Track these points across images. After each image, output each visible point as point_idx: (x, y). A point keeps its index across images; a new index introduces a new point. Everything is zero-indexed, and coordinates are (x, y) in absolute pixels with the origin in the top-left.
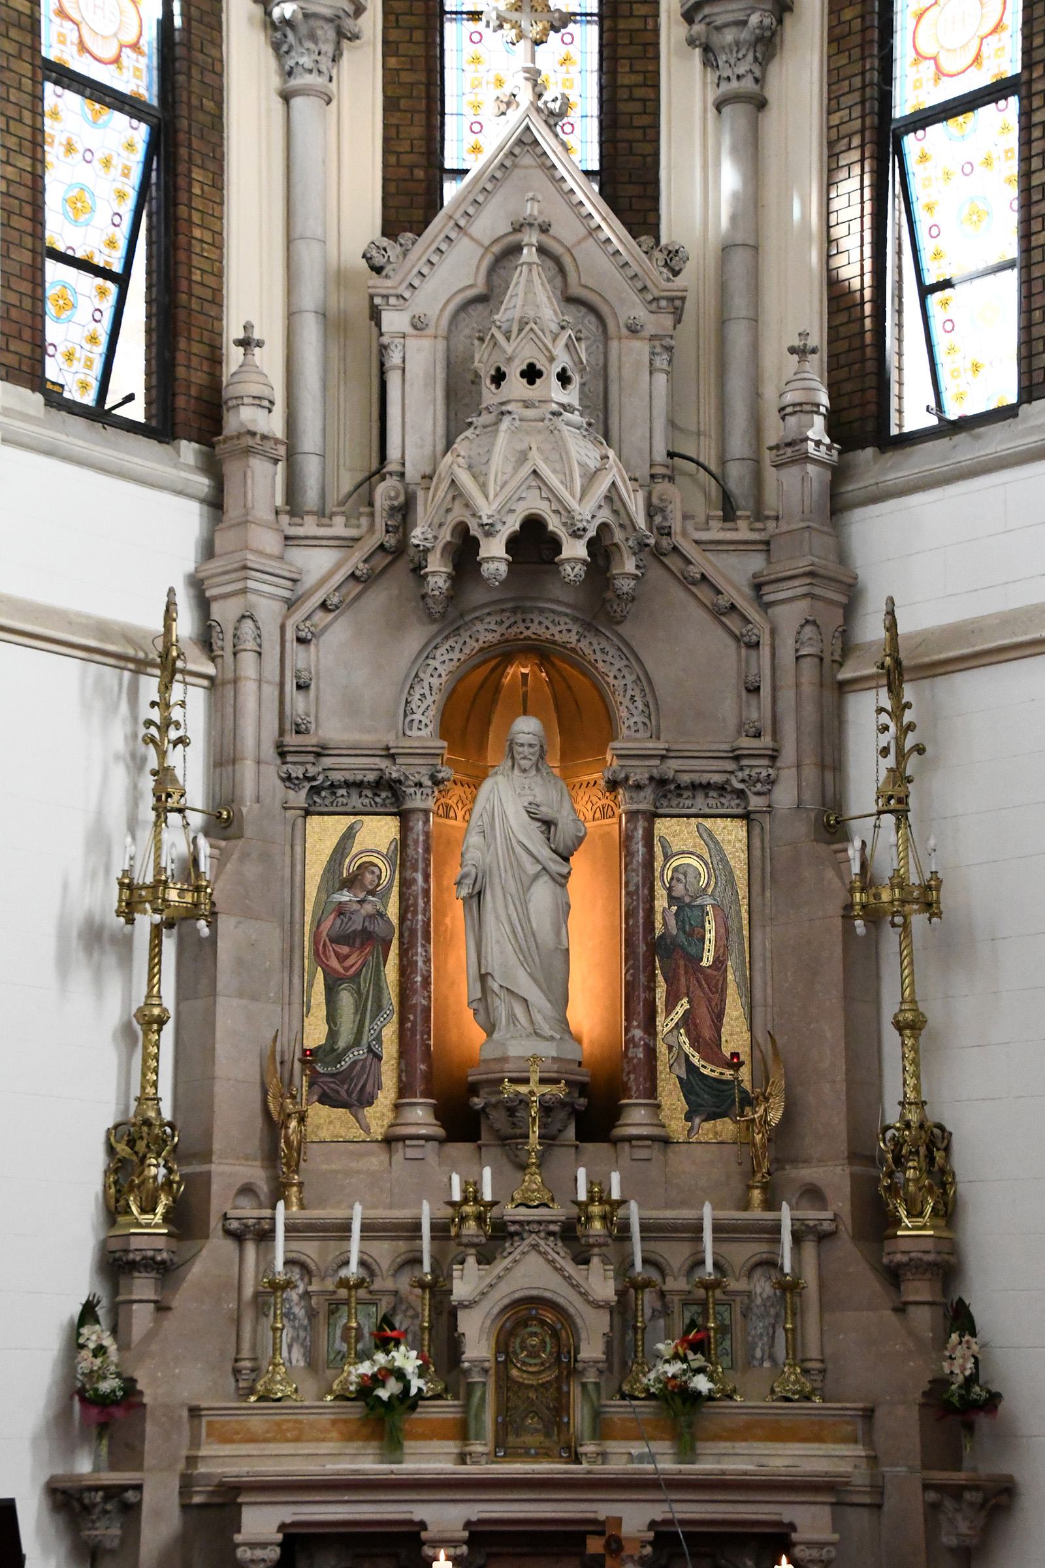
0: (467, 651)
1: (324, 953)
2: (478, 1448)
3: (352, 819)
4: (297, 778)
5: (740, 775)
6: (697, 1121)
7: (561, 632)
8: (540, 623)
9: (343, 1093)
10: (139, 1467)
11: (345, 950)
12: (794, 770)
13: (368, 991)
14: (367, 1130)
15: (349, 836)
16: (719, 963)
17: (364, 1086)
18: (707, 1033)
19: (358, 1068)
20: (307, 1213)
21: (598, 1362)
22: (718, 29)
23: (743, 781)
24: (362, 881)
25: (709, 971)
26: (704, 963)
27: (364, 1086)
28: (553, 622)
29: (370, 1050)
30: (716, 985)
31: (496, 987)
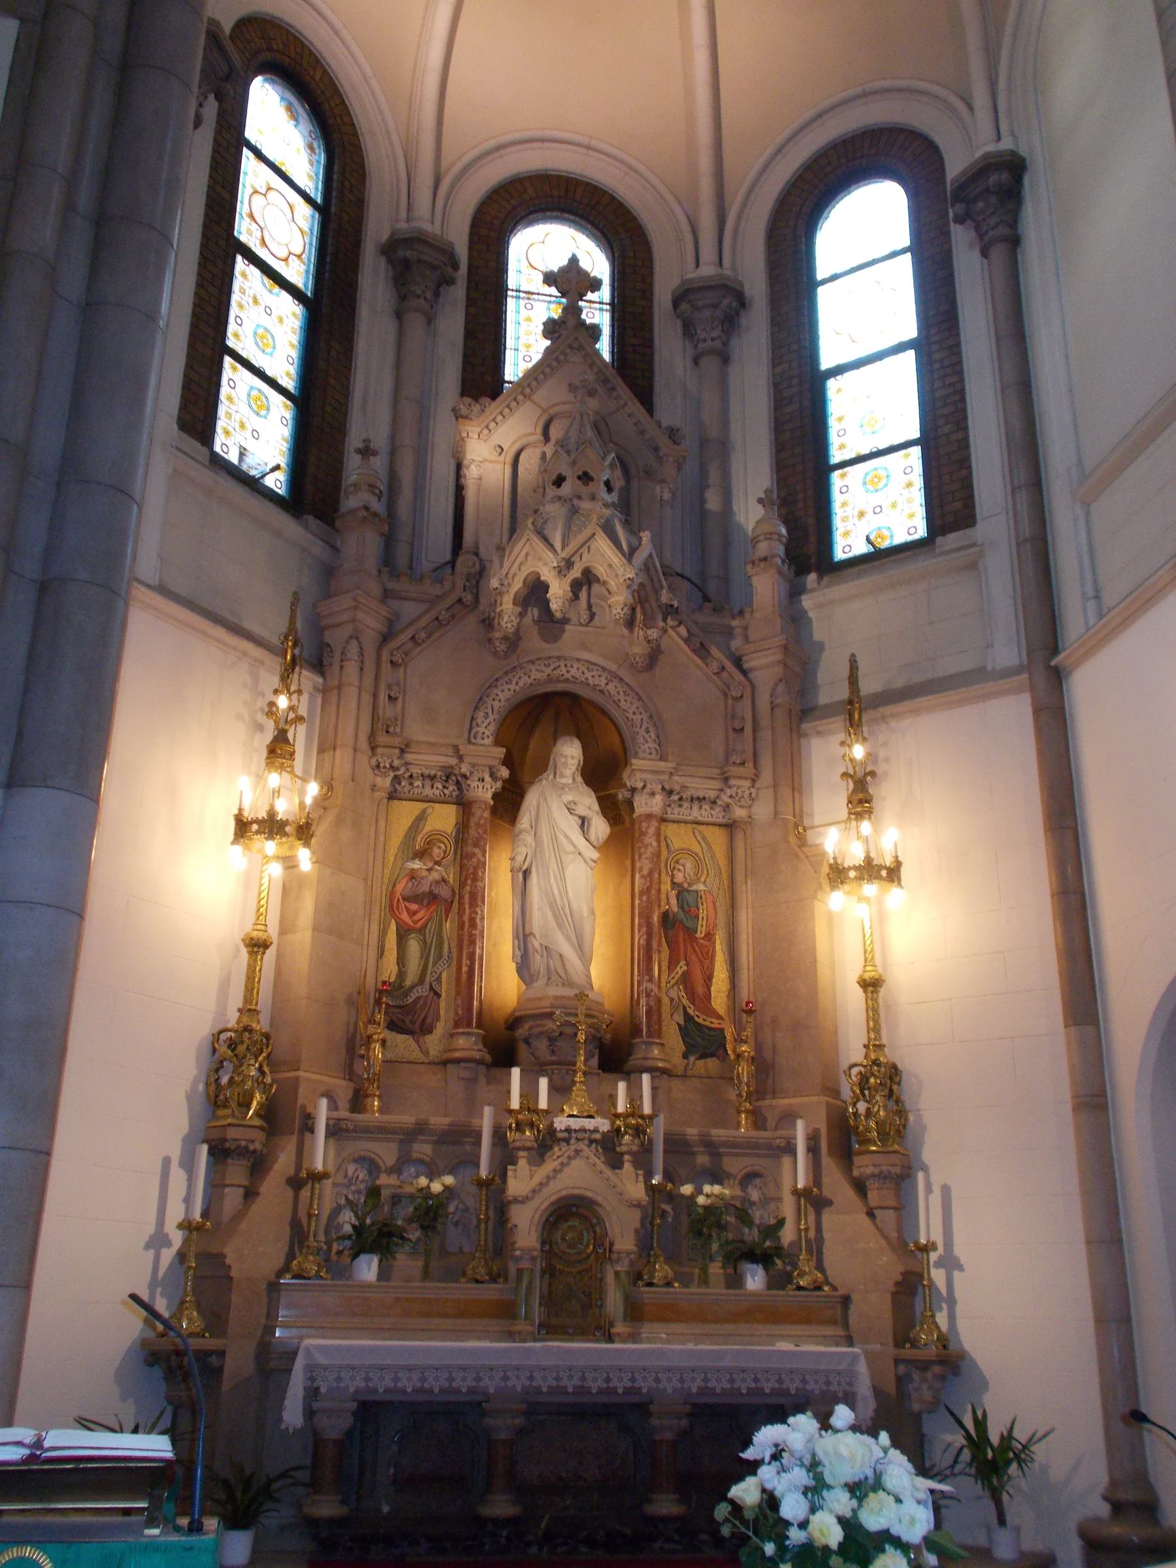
0: (521, 684)
1: (398, 908)
2: (521, 1326)
3: (425, 805)
4: (385, 767)
5: (729, 792)
6: (692, 1059)
7: (593, 676)
8: (578, 669)
9: (407, 1021)
10: (224, 1334)
11: (414, 907)
12: (771, 790)
13: (432, 942)
14: (426, 1053)
15: (422, 817)
16: (709, 936)
17: (426, 1017)
18: (700, 990)
19: (421, 1002)
20: (387, 1118)
21: (631, 1253)
22: (698, 309)
23: (731, 797)
24: (431, 855)
25: (702, 941)
26: (698, 935)
27: (426, 1017)
28: (588, 669)
29: (431, 988)
30: (707, 953)
31: (537, 945)
